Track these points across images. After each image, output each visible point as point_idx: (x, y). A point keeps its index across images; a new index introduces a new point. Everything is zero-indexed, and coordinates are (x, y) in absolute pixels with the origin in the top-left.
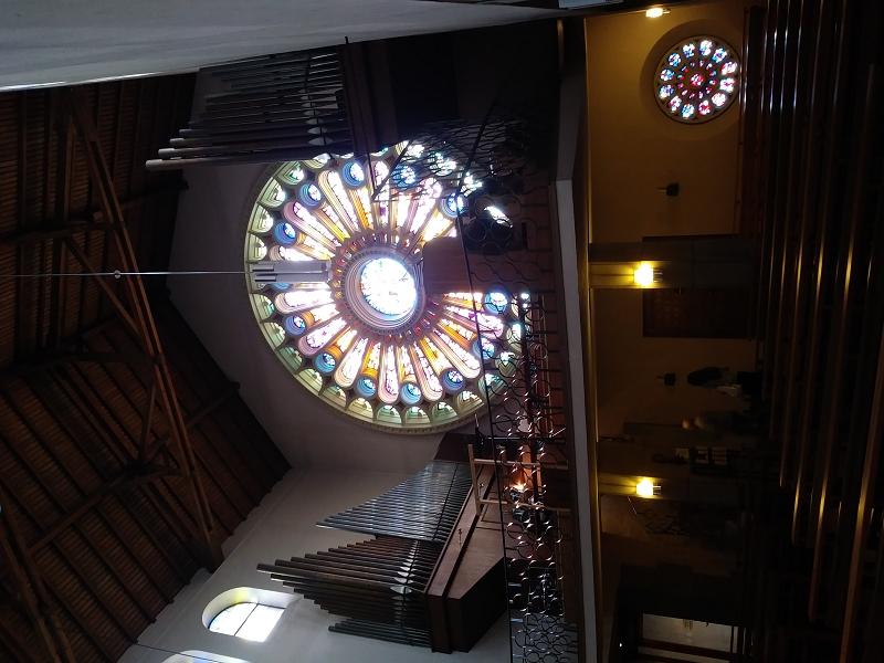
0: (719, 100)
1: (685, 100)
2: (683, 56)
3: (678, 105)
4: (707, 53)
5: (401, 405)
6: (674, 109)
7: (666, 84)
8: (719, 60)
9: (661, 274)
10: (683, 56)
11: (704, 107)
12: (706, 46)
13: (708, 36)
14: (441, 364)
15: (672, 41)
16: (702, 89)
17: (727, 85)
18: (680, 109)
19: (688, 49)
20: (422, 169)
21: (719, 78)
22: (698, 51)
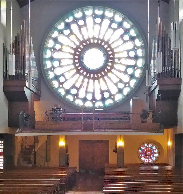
0: (143, 159)
3: (143, 148)
4: (155, 155)
6: (142, 147)
7: (148, 146)
8: (153, 158)
9: (62, 148)
10: (155, 150)
11: (141, 155)
12: (157, 155)
13: (159, 156)
14: (67, 75)
15: (159, 147)
16: (147, 155)
17: (146, 161)
18: (141, 149)
20: (132, 76)
21: (148, 158)
22: (155, 153)
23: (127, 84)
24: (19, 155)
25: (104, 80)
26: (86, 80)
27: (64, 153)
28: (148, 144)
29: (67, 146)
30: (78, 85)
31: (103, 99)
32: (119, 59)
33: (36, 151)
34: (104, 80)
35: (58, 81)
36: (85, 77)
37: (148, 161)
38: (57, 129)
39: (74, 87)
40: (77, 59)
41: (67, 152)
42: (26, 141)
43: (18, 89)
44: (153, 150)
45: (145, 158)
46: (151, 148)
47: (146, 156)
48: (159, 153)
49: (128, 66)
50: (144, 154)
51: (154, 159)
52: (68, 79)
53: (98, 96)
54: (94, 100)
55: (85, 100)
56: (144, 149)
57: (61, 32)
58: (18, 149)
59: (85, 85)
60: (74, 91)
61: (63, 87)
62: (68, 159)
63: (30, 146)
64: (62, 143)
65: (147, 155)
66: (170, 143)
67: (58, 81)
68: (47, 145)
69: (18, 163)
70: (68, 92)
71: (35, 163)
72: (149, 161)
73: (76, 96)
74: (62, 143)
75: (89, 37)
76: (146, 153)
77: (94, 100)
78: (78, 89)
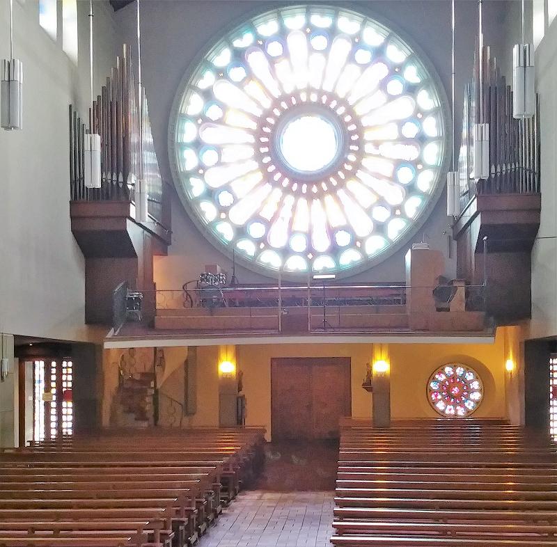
0: (440, 406)
1: (442, 384)
2: (472, 381)
5: (198, 145)
6: (437, 376)
7: (454, 371)
9: (226, 380)
10: (472, 381)
11: (436, 396)
12: (476, 396)
15: (483, 374)
16: (450, 396)
17: (450, 411)
18: (437, 381)
19: (476, 385)
20: (411, 189)
21: (455, 405)
22: (473, 391)
23: (397, 211)
24: (114, 398)
25: (338, 199)
26: (290, 199)
27: (233, 392)
28: (454, 368)
29: (240, 374)
30: (267, 214)
31: (335, 251)
32: (377, 144)
33: (159, 386)
34: (338, 199)
35: (216, 203)
36: (287, 191)
37: (453, 412)
38: (212, 330)
39: (257, 218)
40: (264, 145)
41: (240, 389)
42: (133, 362)
43: (117, 227)
44: (467, 383)
45: (447, 403)
46: (463, 377)
47: (449, 398)
48: (483, 390)
49: (399, 163)
50: (444, 394)
51: (470, 405)
52: (240, 199)
53: (322, 243)
54: (310, 252)
55: (286, 252)
56: (445, 381)
57: (221, 74)
58: (111, 382)
59: (286, 212)
60: (257, 230)
61: (227, 219)
62: (243, 407)
63: (143, 374)
64: (227, 366)
65: (450, 396)
66: (511, 365)
67: (216, 203)
68: (186, 371)
69: (112, 419)
70: (241, 232)
71: (156, 417)
72: (456, 411)
73: (263, 242)
74: (227, 366)
75: (244, 395)
76: (449, 390)
77: (310, 252)
78: (268, 224)
